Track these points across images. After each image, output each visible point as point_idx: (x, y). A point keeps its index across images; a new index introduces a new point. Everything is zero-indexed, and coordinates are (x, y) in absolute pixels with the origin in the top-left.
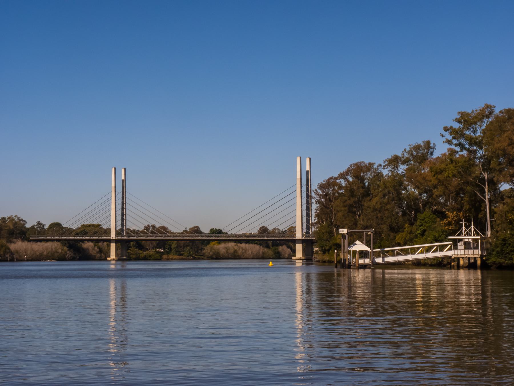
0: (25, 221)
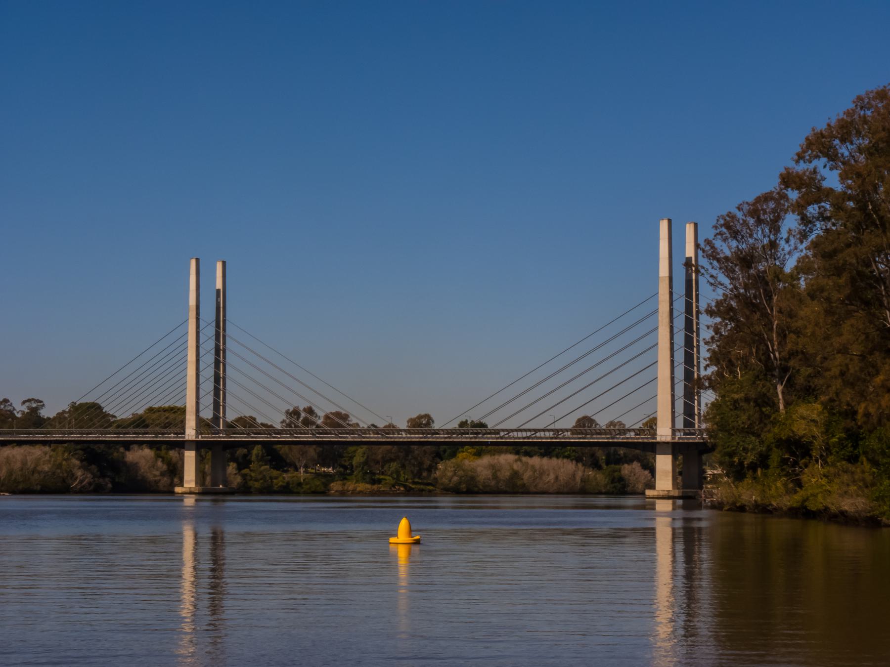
0: (41, 402)
